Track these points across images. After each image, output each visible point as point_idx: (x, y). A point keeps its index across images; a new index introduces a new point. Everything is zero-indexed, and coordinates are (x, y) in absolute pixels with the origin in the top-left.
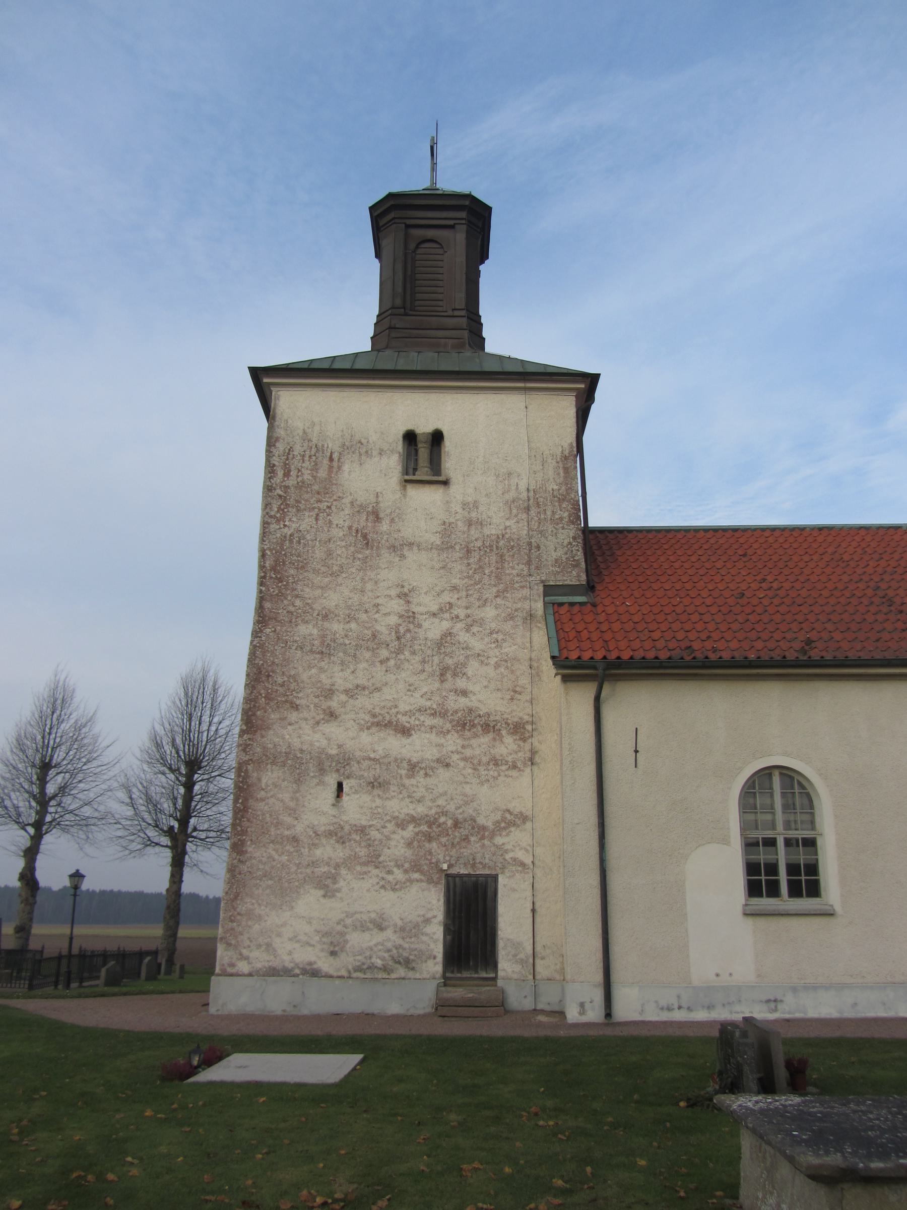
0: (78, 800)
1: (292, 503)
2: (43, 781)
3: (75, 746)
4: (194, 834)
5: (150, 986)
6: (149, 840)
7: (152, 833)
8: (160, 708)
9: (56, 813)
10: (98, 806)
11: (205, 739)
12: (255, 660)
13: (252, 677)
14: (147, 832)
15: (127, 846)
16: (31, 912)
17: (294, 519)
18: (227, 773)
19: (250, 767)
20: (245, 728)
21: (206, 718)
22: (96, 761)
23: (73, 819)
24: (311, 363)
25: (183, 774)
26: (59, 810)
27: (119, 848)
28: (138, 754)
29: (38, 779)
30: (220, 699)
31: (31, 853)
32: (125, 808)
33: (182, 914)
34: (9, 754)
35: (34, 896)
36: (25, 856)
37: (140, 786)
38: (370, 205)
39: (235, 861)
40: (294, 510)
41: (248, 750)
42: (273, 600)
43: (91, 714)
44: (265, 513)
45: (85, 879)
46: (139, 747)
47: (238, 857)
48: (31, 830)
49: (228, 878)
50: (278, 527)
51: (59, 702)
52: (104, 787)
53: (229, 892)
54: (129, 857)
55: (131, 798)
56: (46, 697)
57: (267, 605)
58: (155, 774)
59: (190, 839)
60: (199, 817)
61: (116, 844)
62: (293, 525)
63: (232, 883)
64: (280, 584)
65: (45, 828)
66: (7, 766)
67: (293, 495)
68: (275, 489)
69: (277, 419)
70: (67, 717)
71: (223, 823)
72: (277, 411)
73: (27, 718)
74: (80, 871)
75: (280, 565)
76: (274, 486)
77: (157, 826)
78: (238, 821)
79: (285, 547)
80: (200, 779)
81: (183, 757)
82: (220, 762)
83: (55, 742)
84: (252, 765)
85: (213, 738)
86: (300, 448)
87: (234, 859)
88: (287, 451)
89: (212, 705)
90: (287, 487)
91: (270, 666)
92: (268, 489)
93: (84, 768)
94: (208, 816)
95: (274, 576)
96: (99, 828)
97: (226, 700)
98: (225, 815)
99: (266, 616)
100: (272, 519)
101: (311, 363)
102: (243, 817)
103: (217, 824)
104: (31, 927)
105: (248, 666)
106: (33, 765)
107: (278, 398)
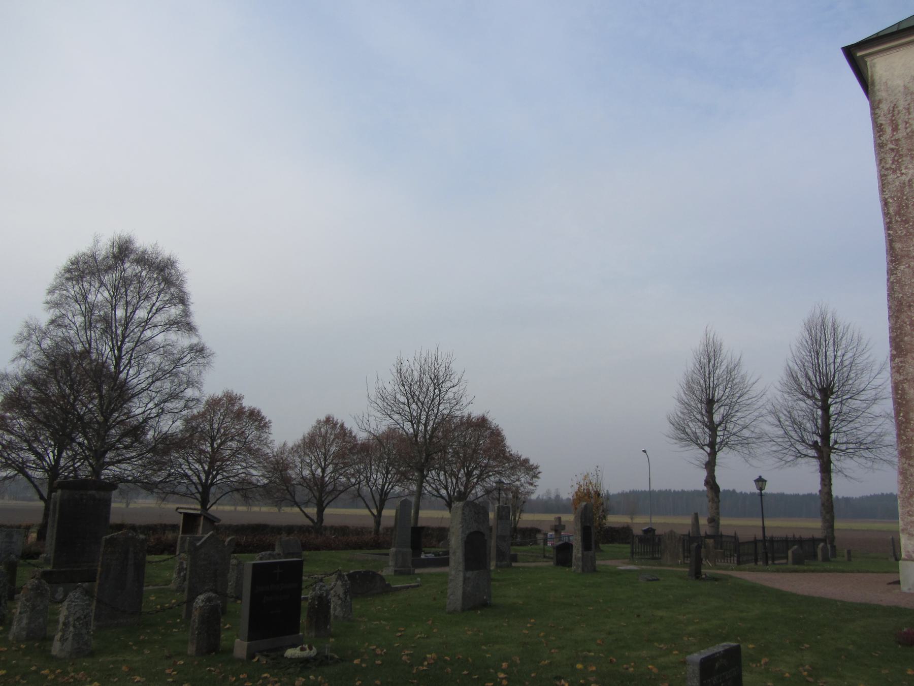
0: (737, 425)
1: (905, 153)
2: (710, 413)
3: (729, 385)
4: (836, 446)
5: (827, 566)
6: (800, 453)
7: (800, 447)
8: (791, 349)
9: (724, 435)
10: (754, 429)
11: (832, 370)
12: (894, 294)
13: (895, 309)
14: (796, 446)
15: (783, 458)
16: (717, 508)
17: (910, 166)
18: (856, 396)
19: (905, 386)
20: (895, 353)
21: (830, 353)
22: (746, 395)
23: (737, 439)
24: (899, 25)
25: (818, 399)
26: (726, 433)
27: (777, 460)
28: (779, 387)
29: (707, 412)
30: (841, 335)
31: (710, 465)
32: (776, 429)
33: (835, 510)
34: (683, 395)
35: (717, 497)
36: (706, 468)
37: (785, 412)
39: (906, 465)
40: (909, 158)
41: (901, 371)
42: (903, 240)
43: (737, 360)
44: (880, 168)
45: (767, 483)
46: (779, 382)
47: (907, 462)
48: (708, 449)
49: (901, 480)
50: (896, 176)
51: (712, 354)
52: (756, 414)
53: (904, 491)
54: (785, 466)
55: (780, 421)
56: (701, 351)
57: (898, 246)
58: (795, 401)
59: (833, 451)
60: (838, 432)
61: (774, 457)
62: (910, 172)
63: (906, 484)
64: (907, 226)
65: (717, 447)
66: (683, 404)
67: (904, 145)
68: (886, 145)
69: (876, 84)
70: (719, 364)
71: (860, 436)
72: (875, 77)
73: (691, 369)
74: (762, 477)
75: (903, 209)
76: (885, 142)
77: (804, 441)
78: (902, 432)
79: (906, 193)
80: (834, 402)
81: (816, 386)
82: (847, 387)
83: (713, 384)
84: (907, 383)
85: (839, 369)
86: (904, 102)
87: (904, 464)
88: (892, 109)
89: (834, 342)
90: (897, 140)
91: (909, 297)
92: (880, 146)
93: (739, 401)
94: (844, 432)
95: (899, 219)
96: (757, 445)
97: (846, 336)
98: (860, 430)
99: (898, 255)
100: (889, 171)
101: (899, 25)
102: (906, 428)
103: (855, 438)
104: (719, 519)
105: (888, 301)
106: (701, 402)
107: (873, 66)
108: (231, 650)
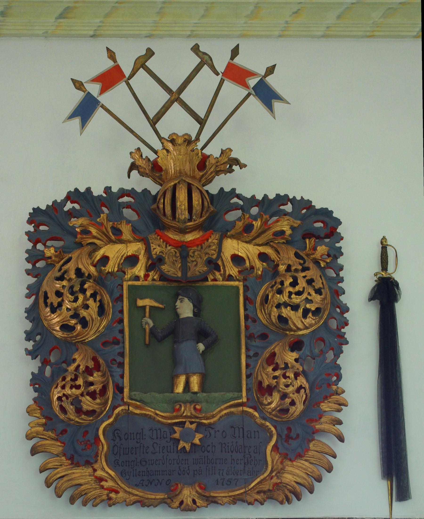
38: (135, 189)
108: (50, 361)
